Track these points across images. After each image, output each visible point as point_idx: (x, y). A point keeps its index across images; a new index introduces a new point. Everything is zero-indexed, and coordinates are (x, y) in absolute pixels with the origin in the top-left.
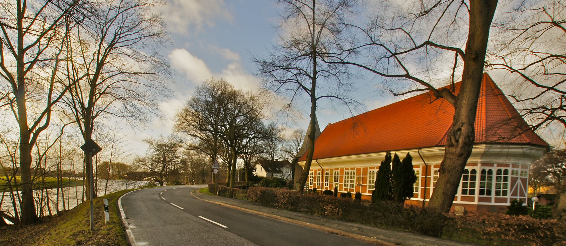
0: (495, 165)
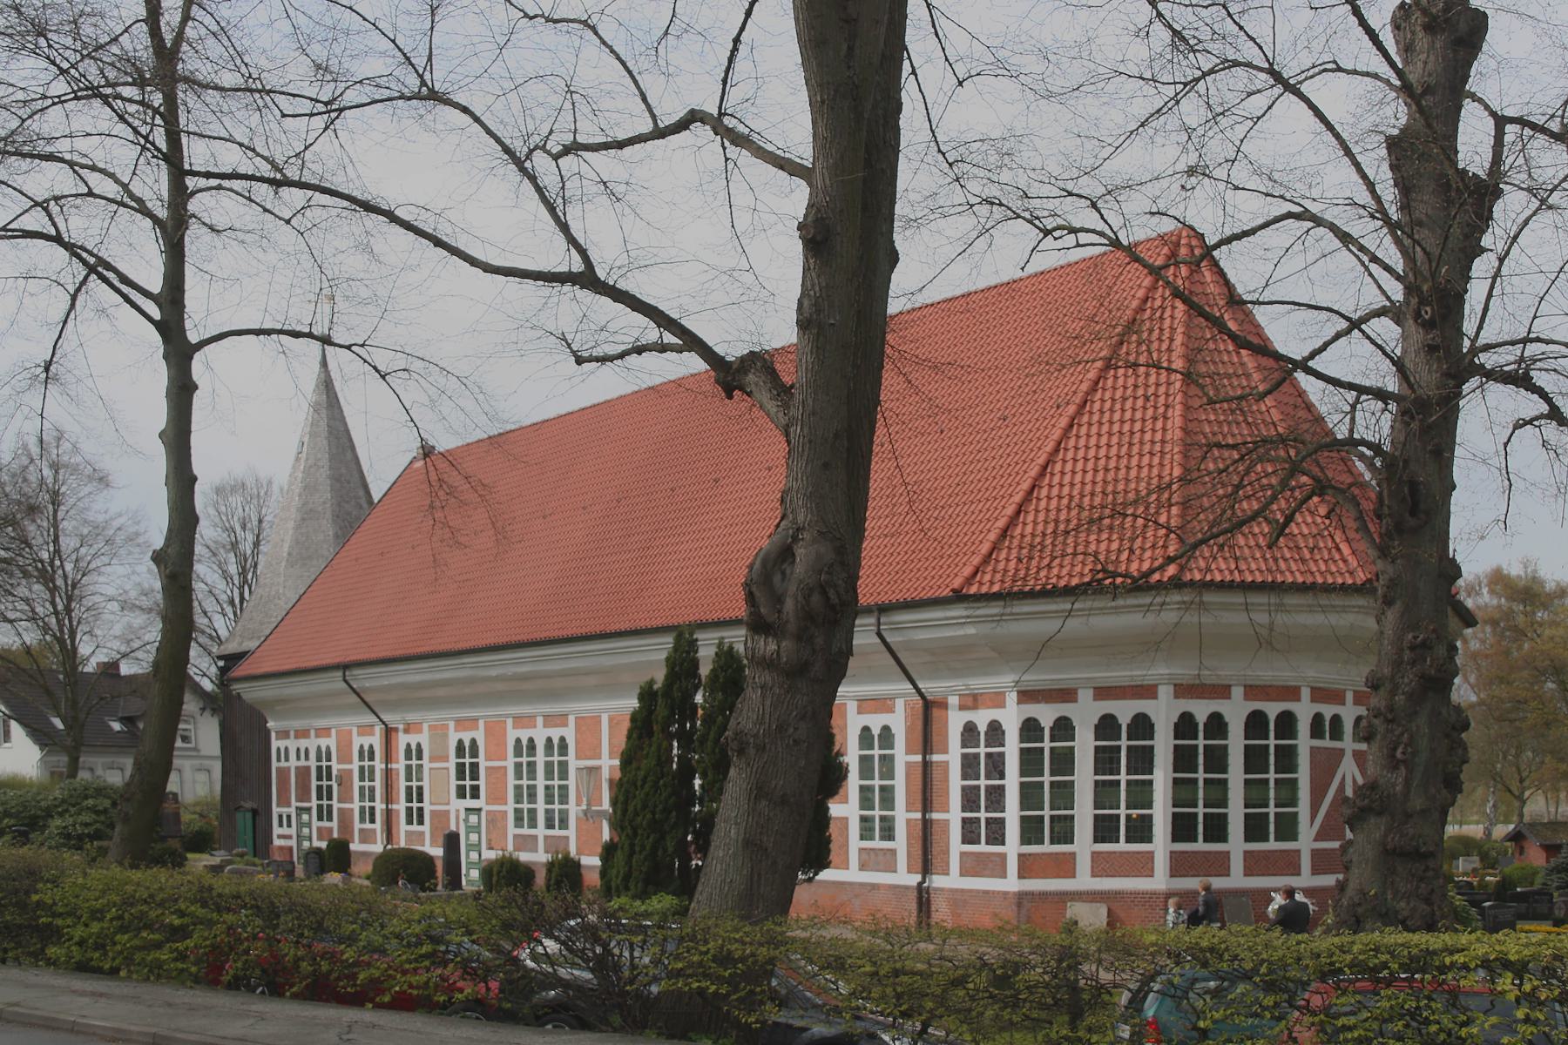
0: (1085, 695)
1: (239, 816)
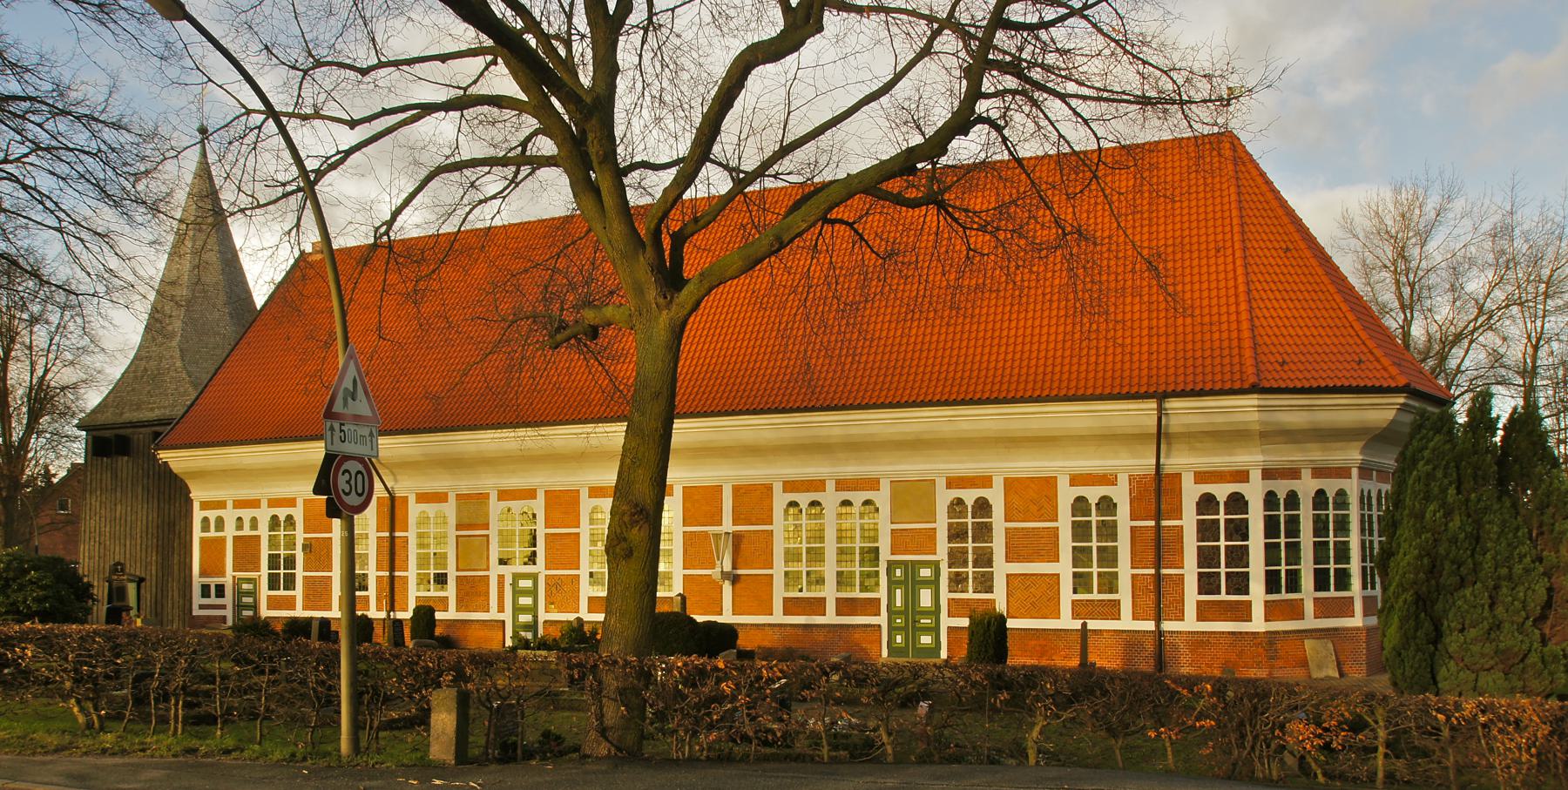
0: (1306, 474)
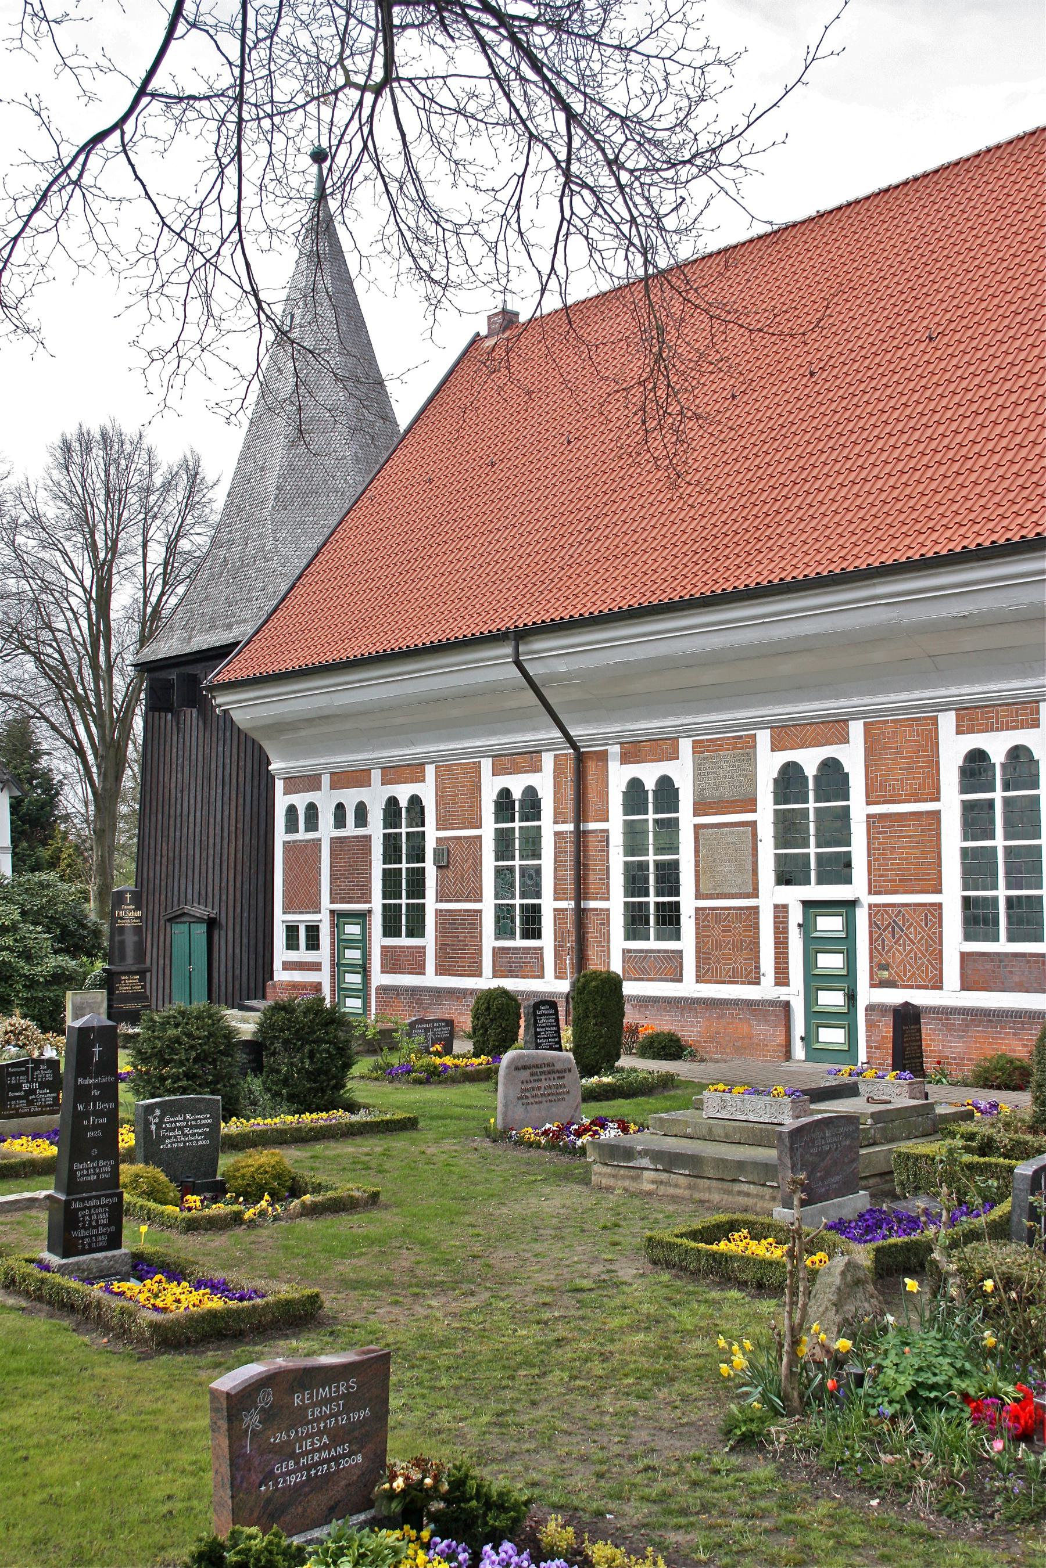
1: (179, 930)
